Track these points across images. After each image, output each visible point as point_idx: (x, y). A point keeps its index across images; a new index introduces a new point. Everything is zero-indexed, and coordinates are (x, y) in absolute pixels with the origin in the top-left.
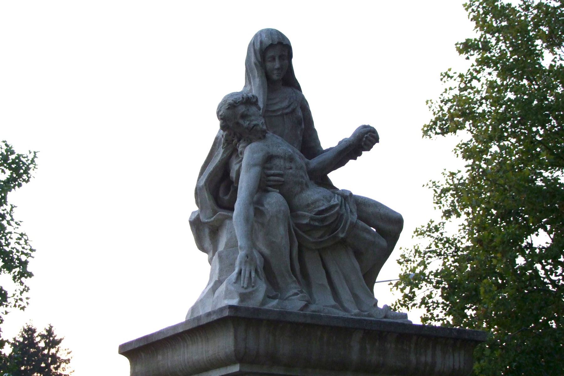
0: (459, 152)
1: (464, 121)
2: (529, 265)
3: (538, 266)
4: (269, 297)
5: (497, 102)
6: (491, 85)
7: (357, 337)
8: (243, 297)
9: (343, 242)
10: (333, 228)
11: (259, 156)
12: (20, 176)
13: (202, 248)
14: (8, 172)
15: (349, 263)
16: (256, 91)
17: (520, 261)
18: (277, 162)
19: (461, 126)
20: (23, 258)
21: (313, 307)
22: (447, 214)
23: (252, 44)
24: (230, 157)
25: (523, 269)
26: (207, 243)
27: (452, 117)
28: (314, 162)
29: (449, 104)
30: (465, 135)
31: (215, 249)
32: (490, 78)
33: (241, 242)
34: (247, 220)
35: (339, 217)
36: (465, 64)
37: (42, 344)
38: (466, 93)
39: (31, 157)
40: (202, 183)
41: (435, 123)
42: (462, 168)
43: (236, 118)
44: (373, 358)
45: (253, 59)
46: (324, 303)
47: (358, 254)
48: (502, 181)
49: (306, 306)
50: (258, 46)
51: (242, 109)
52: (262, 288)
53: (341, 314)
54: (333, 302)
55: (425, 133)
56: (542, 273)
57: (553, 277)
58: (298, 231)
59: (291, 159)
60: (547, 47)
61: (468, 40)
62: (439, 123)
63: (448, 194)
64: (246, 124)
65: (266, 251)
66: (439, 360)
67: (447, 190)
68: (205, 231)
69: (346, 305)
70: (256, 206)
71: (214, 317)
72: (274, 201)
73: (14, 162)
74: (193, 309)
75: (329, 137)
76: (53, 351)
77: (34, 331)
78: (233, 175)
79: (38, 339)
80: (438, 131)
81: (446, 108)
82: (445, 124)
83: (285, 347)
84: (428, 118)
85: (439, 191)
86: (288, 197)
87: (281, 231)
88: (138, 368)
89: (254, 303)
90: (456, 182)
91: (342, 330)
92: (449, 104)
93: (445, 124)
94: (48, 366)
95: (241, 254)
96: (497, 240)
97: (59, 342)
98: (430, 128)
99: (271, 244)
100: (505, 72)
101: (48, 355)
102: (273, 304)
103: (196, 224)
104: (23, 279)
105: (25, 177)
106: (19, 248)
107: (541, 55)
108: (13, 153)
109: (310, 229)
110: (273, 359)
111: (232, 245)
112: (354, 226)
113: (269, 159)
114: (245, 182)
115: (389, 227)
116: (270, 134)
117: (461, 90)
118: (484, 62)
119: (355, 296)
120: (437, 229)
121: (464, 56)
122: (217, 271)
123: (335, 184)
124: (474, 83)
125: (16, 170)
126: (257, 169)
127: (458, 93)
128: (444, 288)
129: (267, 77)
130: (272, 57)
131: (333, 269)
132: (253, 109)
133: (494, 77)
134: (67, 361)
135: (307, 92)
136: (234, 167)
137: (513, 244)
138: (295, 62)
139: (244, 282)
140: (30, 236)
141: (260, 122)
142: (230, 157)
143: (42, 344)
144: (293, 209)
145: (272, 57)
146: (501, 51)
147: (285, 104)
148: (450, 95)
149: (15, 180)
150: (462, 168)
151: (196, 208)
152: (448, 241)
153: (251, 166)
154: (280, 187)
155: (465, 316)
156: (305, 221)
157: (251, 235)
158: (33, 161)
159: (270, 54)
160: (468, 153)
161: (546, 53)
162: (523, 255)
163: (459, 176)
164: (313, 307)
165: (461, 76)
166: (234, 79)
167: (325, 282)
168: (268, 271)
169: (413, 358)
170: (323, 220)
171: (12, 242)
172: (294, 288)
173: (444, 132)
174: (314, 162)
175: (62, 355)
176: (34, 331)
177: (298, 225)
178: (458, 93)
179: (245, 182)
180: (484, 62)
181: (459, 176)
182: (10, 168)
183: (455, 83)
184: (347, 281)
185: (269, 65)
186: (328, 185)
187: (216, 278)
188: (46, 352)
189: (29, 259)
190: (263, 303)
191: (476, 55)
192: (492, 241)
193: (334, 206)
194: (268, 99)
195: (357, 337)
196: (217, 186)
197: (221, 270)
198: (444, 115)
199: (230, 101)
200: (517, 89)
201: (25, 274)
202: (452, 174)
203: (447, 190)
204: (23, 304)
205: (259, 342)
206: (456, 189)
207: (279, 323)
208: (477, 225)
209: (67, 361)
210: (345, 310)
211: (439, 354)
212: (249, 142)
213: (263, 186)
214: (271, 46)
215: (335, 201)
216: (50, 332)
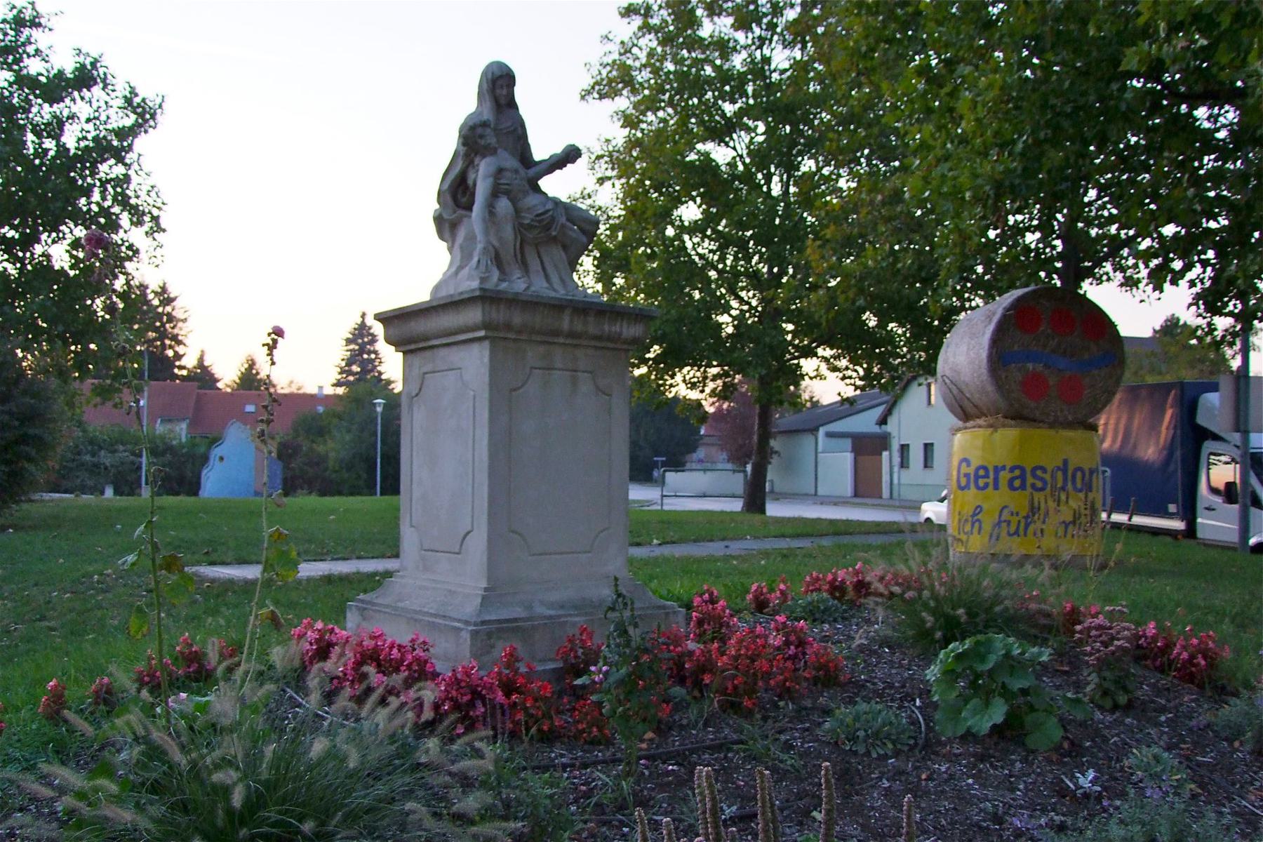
0: (615, 119)
1: (623, 88)
2: (678, 237)
3: (686, 237)
4: (501, 280)
5: (656, 72)
6: (651, 54)
7: (568, 312)
8: (483, 280)
9: (555, 239)
10: (548, 228)
11: (493, 169)
12: (146, 121)
13: (441, 237)
14: (133, 117)
15: (558, 254)
16: (487, 115)
17: (670, 232)
18: (508, 174)
19: (617, 93)
20: (155, 212)
21: (533, 289)
22: (601, 181)
23: (484, 74)
24: (467, 167)
25: (673, 240)
26: (447, 235)
27: (610, 81)
28: (532, 172)
29: (609, 68)
30: (623, 102)
31: (453, 242)
32: (650, 44)
33: (480, 237)
34: (484, 220)
35: (553, 219)
36: (627, 29)
37: (156, 302)
38: (624, 58)
39: (158, 101)
40: (446, 186)
41: (593, 88)
42: (620, 136)
43: (473, 140)
44: (579, 327)
45: (485, 86)
46: (539, 286)
47: (565, 247)
48: (657, 155)
49: (528, 288)
50: (490, 76)
51: (479, 131)
52: (496, 274)
53: (553, 294)
54: (545, 285)
55: (583, 98)
56: (689, 245)
57: (700, 250)
58: (520, 228)
59: (516, 171)
60: (708, 16)
61: (630, 5)
62: (597, 88)
63: (602, 161)
64: (482, 142)
65: (496, 244)
66: (624, 330)
67: (601, 157)
68: (446, 226)
69: (556, 286)
70: (490, 208)
71: (466, 296)
72: (504, 205)
73: (139, 106)
74: (437, 288)
75: (540, 151)
76: (168, 309)
77: (147, 287)
78: (470, 182)
79: (151, 296)
80: (596, 96)
81: (604, 72)
82: (605, 89)
83: (517, 319)
84: (587, 82)
85: (593, 157)
86: (514, 201)
87: (508, 232)
88: (391, 331)
89: (490, 285)
90: (611, 149)
91: (558, 307)
92: (609, 68)
93: (605, 89)
94: (163, 325)
95: (480, 246)
96: (649, 213)
97: (173, 300)
98: (589, 93)
99: (500, 239)
100: (667, 40)
101: (163, 314)
102: (504, 286)
103: (439, 220)
104: (156, 235)
105: (152, 123)
106: (150, 201)
107: (700, 25)
108: (136, 95)
109: (530, 227)
110: (508, 327)
111: (471, 238)
112: (563, 226)
113: (500, 171)
114: (482, 190)
115: (588, 227)
116: (499, 151)
117: (621, 54)
118: (646, 28)
119: (563, 281)
120: (590, 197)
121: (627, 20)
122: (459, 258)
123: (543, 189)
124: (635, 50)
125: (141, 115)
126: (491, 179)
127: (616, 56)
128: (595, 258)
129: (496, 101)
130: (499, 85)
131: (546, 259)
132: (488, 131)
133: (654, 44)
134: (184, 321)
135: (523, 111)
136: (471, 176)
137: (665, 216)
138: (516, 89)
139: (482, 268)
140: (160, 186)
141: (492, 140)
142: (467, 167)
143: (156, 302)
144: (517, 211)
145: (499, 85)
146: (664, 21)
147: (509, 124)
148: (609, 60)
149: (140, 126)
150: (620, 136)
151: (437, 206)
152: (600, 208)
153: (486, 177)
154: (507, 193)
155: (614, 285)
156: (527, 222)
157: (486, 232)
158: (160, 106)
159: (499, 82)
160: (629, 122)
161: (706, 21)
162: (673, 225)
163: (614, 143)
164: (533, 289)
165: (622, 43)
166: (465, 101)
167: (540, 268)
168: (498, 260)
169: (606, 328)
170: (539, 222)
171: (143, 194)
172: (517, 273)
173: (601, 97)
174: (532, 172)
175: (178, 314)
176: (147, 287)
177: (521, 225)
178: (616, 56)
179: (482, 190)
180: (646, 28)
181: (614, 143)
182: (135, 113)
183: (615, 48)
184: (556, 266)
185: (498, 91)
186: (537, 189)
187: (457, 263)
188: (160, 310)
189: (161, 213)
190: (497, 285)
191: (637, 21)
192: (644, 213)
193: (548, 211)
194: (497, 119)
195: (568, 312)
196: (456, 192)
197: (462, 258)
198: (602, 80)
199: (471, 124)
200: (678, 61)
201: (157, 227)
202: (608, 141)
203: (601, 157)
204: (157, 261)
205: (499, 315)
206: (611, 156)
207: (514, 301)
208: (630, 193)
209: (184, 321)
210: (555, 290)
211: (625, 325)
212: (484, 156)
213: (495, 193)
214: (501, 77)
215: (550, 206)
216: (164, 289)
